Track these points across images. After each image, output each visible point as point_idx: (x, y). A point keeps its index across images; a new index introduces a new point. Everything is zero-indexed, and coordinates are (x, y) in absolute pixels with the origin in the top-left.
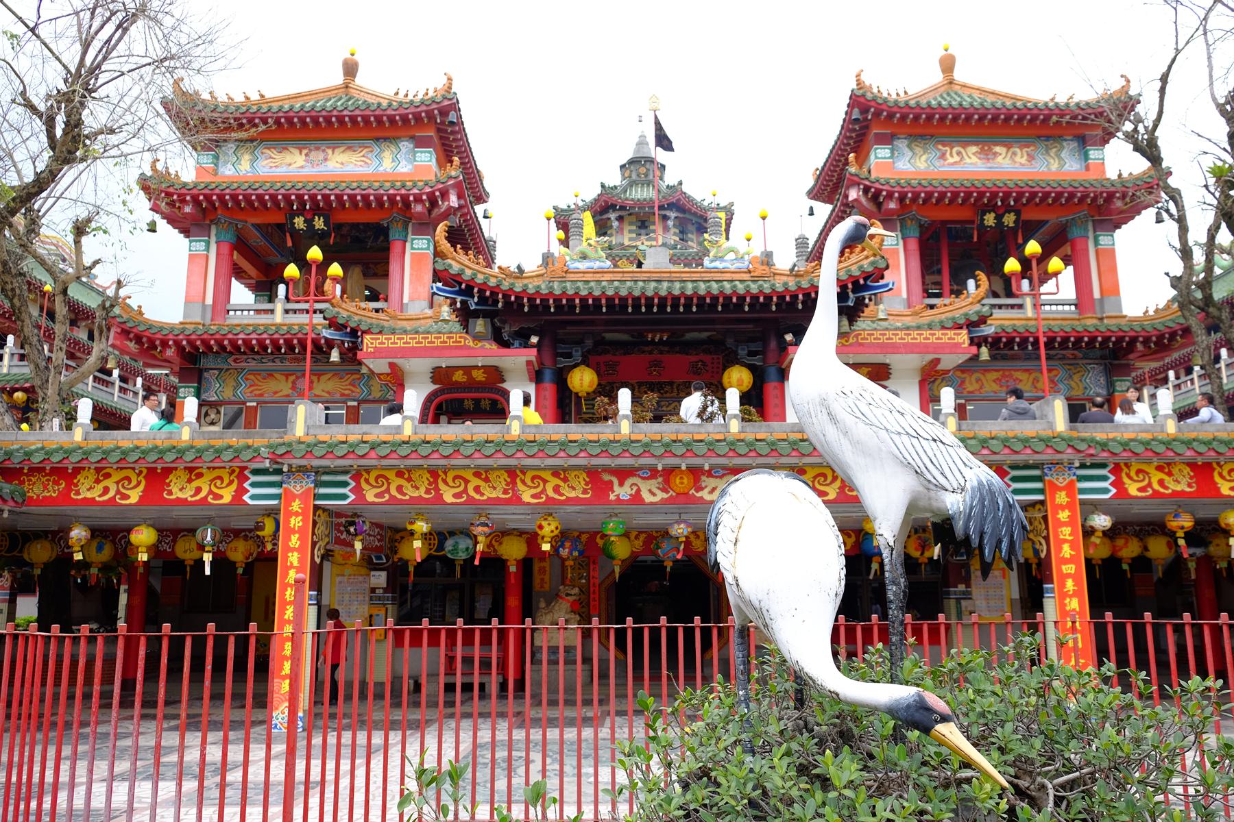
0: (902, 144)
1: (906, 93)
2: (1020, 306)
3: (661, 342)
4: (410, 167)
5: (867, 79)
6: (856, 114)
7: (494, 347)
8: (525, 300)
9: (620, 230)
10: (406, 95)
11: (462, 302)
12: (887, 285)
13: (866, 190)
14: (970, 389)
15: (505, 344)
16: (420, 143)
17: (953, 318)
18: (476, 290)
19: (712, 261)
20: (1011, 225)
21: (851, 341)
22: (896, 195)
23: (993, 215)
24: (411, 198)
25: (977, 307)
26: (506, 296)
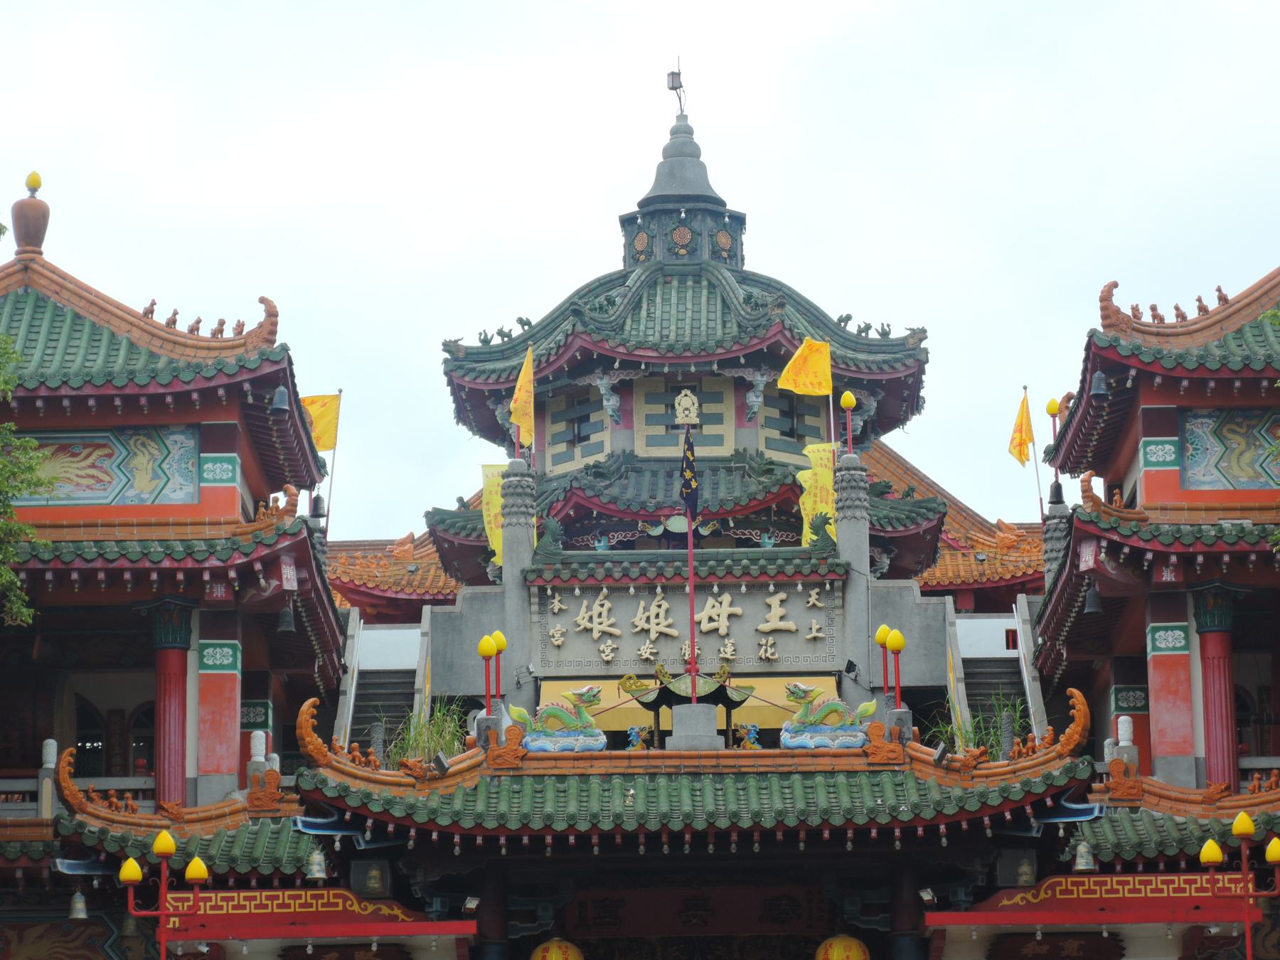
0: (1201, 429)
4: (190, 489)
9: (624, 417)
11: (343, 840)
12: (1090, 811)
13: (1114, 549)
15: (415, 907)
16: (212, 440)
18: (370, 822)
21: (1042, 895)
22: (1174, 559)
24: (206, 577)
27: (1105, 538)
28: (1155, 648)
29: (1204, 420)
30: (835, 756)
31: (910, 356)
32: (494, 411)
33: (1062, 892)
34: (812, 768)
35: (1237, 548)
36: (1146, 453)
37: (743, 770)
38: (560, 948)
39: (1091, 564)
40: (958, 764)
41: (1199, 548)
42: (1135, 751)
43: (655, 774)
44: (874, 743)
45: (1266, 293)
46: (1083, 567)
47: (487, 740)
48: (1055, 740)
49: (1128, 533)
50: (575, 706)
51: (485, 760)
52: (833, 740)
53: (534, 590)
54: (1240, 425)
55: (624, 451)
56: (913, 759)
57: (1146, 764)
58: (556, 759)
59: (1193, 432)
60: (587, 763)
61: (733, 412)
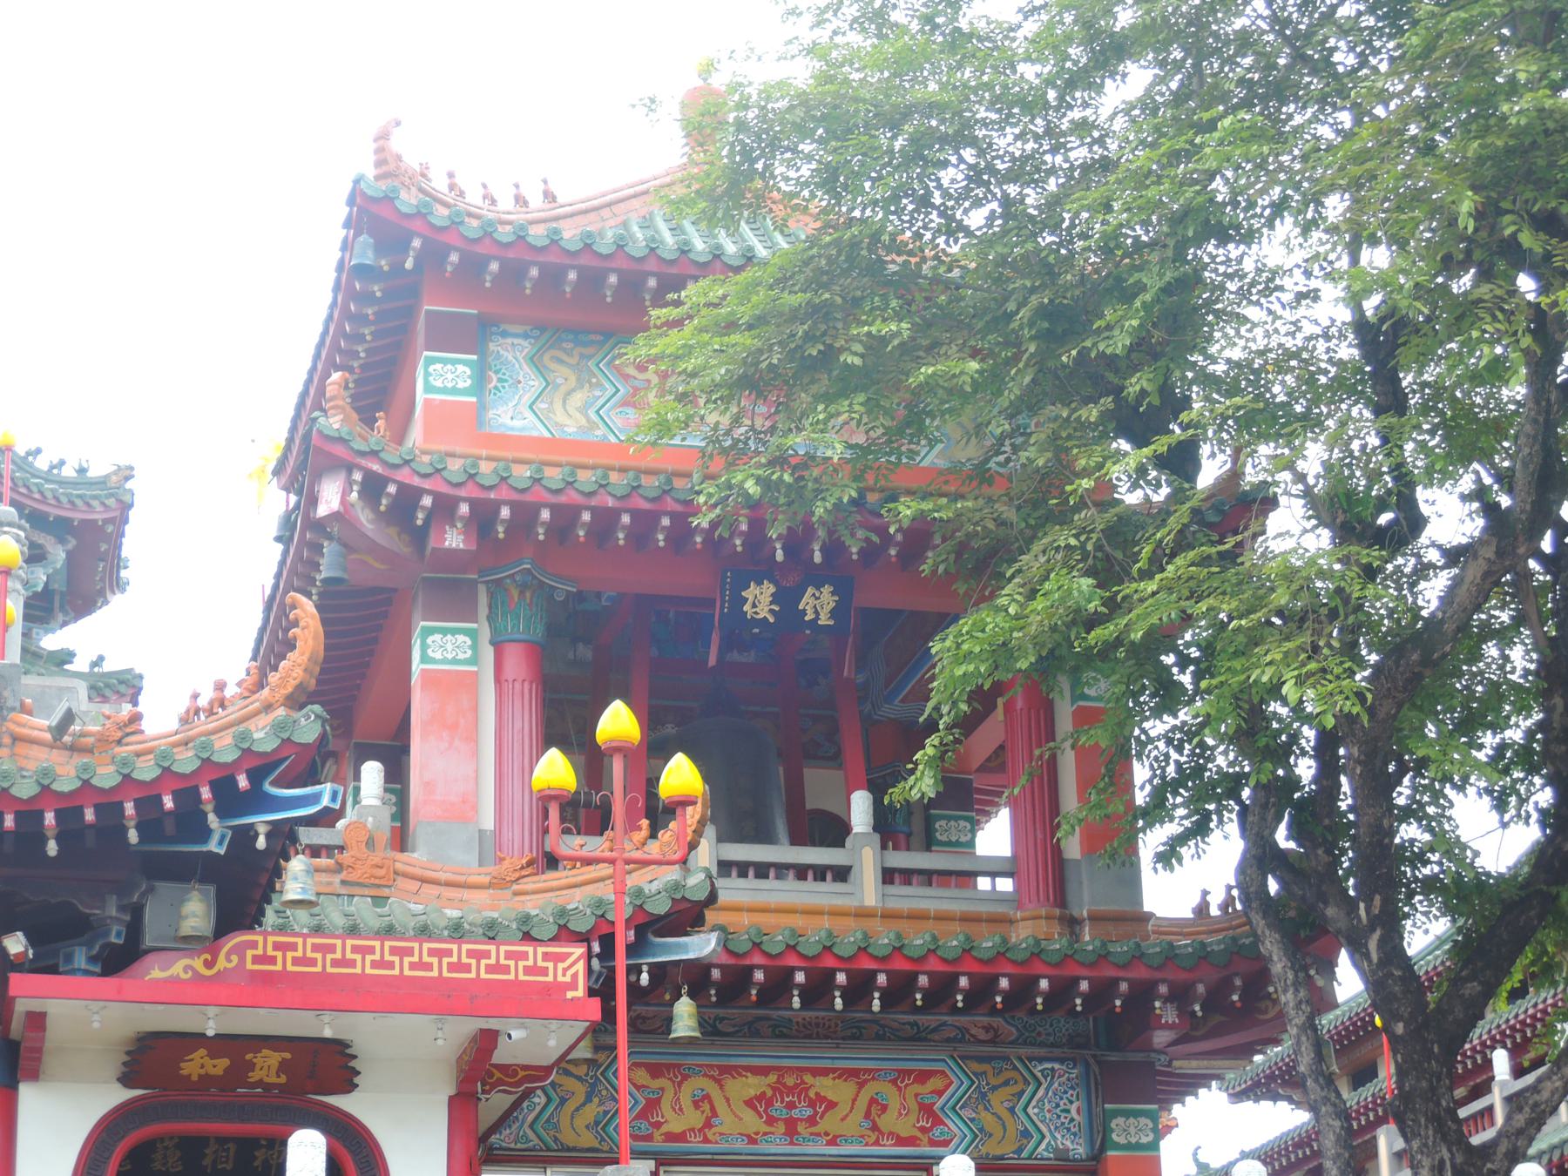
0: (512, 352)
1: (549, 196)
2: (842, 874)
5: (411, 150)
6: (365, 254)
10: (520, 200)
13: (372, 487)
14: (675, 1125)
17: (563, 912)
20: (824, 620)
21: (222, 963)
22: (464, 509)
23: (769, 589)
25: (672, 874)
27: (360, 468)
28: (425, 658)
29: (516, 341)
31: (112, 495)
33: (256, 960)
35: (562, 499)
36: (427, 374)
39: (335, 505)
40: (91, 740)
41: (504, 494)
42: (386, 814)
45: (609, 205)
46: (322, 511)
48: (260, 685)
49: (397, 461)
54: (568, 353)
56: (16, 739)
57: (401, 839)
59: (498, 356)
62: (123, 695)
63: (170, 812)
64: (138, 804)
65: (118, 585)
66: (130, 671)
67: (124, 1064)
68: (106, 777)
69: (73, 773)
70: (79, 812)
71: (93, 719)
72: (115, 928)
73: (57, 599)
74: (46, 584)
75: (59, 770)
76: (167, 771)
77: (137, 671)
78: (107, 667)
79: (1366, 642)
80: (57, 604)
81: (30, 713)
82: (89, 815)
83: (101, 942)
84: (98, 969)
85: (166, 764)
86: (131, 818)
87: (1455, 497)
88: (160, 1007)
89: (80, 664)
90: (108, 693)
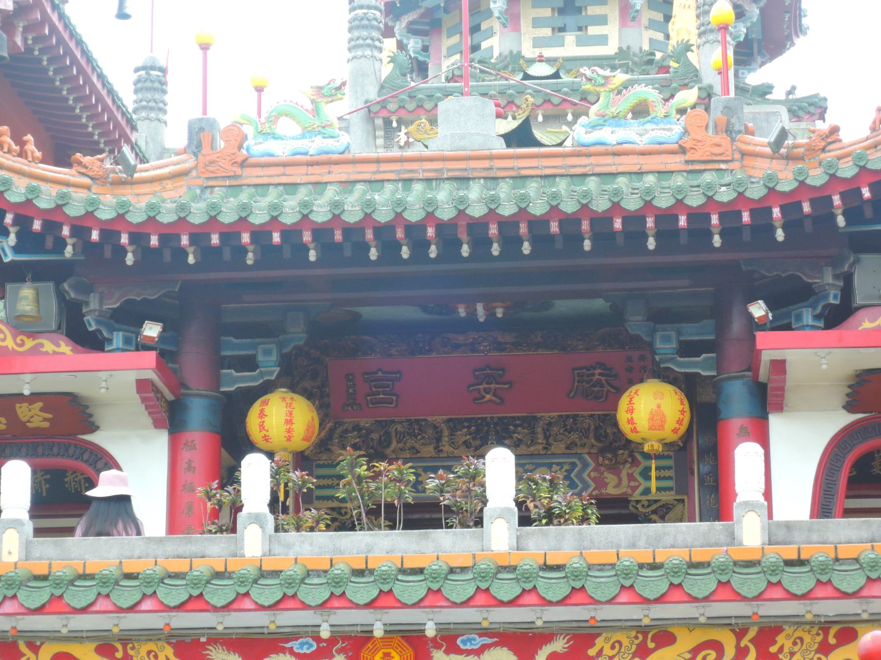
3: (492, 322)
7: (65, 348)
8: (124, 239)
15: (89, 341)
19: (594, 127)
26: (80, 229)
30: (643, 153)
32: (393, 28)
34: (613, 169)
37: (524, 172)
38: (284, 399)
40: (802, 150)
43: (411, 180)
44: (693, 135)
47: (199, 146)
50: (313, 102)
51: (196, 167)
52: (641, 135)
53: (379, 122)
55: (511, 52)
56: (744, 154)
58: (285, 164)
60: (324, 169)
61: (617, 13)
62: (813, 115)
63: (868, 201)
64: (843, 196)
65: (799, 29)
66: (816, 96)
67: (847, 395)
68: (817, 177)
69: (791, 176)
70: (799, 205)
71: (800, 135)
72: (832, 293)
73: (755, 46)
74: (746, 35)
75: (781, 175)
76: (863, 169)
77: (822, 95)
78: (799, 94)
79: (70, 286)
80: (755, 50)
81: (752, 134)
82: (806, 208)
83: (822, 303)
84: (821, 324)
85: (862, 164)
86: (838, 207)
87: (831, 118)
88: (873, 350)
89: (778, 94)
90: (801, 113)
